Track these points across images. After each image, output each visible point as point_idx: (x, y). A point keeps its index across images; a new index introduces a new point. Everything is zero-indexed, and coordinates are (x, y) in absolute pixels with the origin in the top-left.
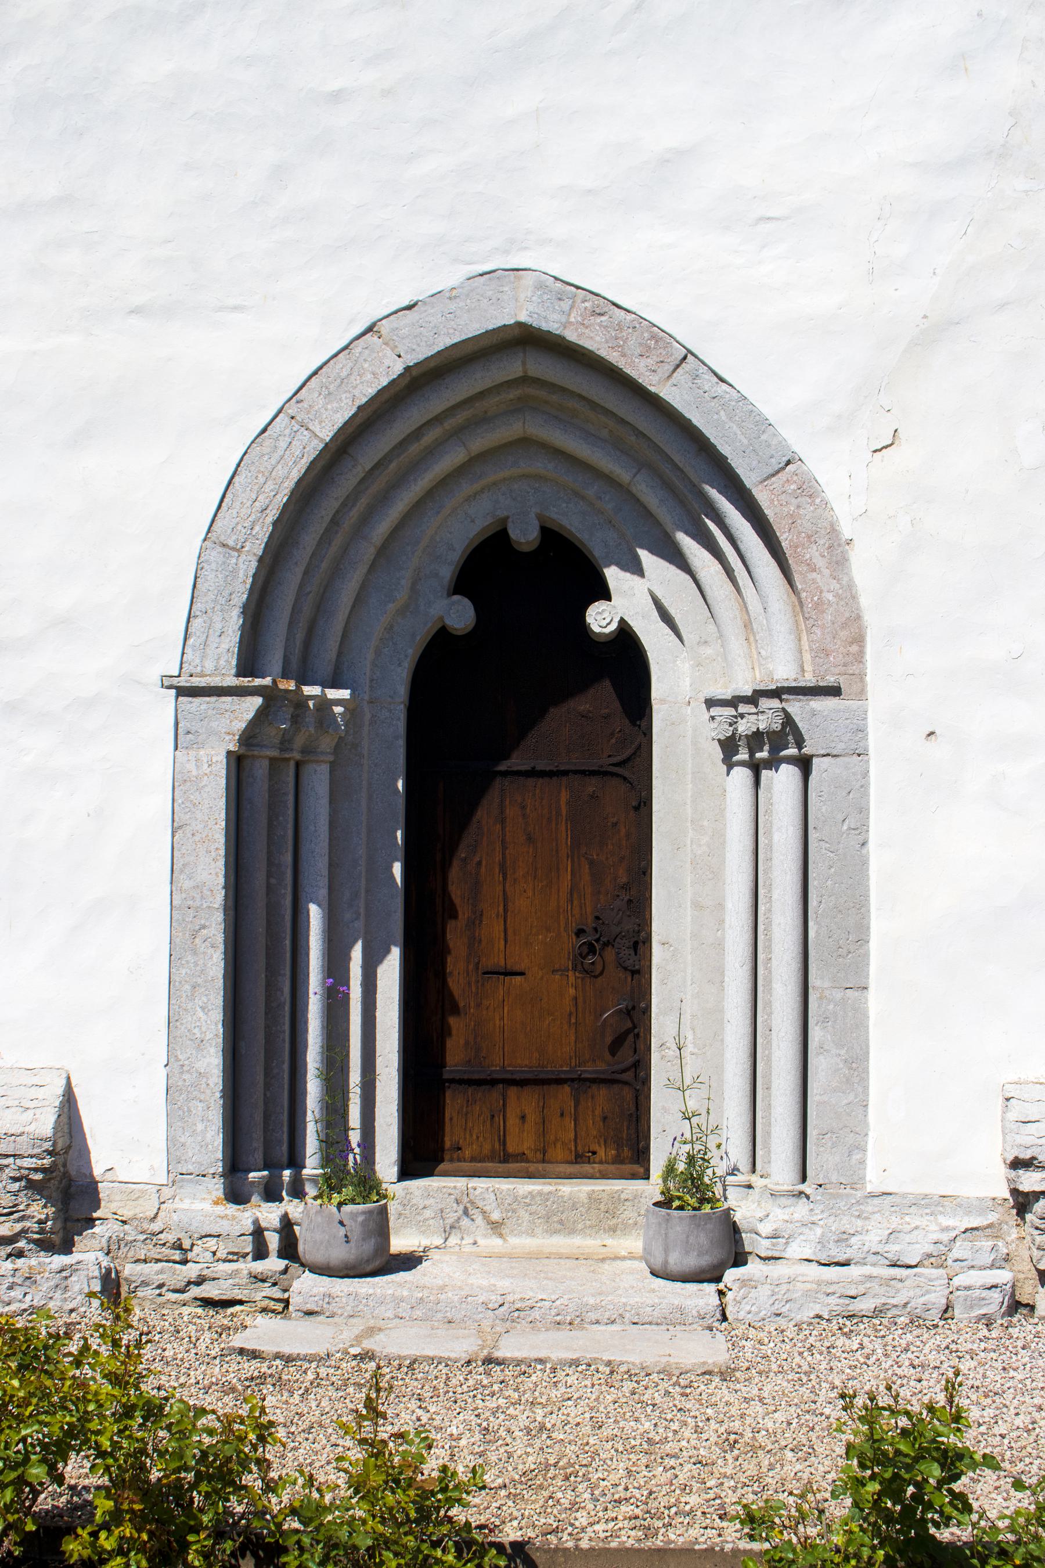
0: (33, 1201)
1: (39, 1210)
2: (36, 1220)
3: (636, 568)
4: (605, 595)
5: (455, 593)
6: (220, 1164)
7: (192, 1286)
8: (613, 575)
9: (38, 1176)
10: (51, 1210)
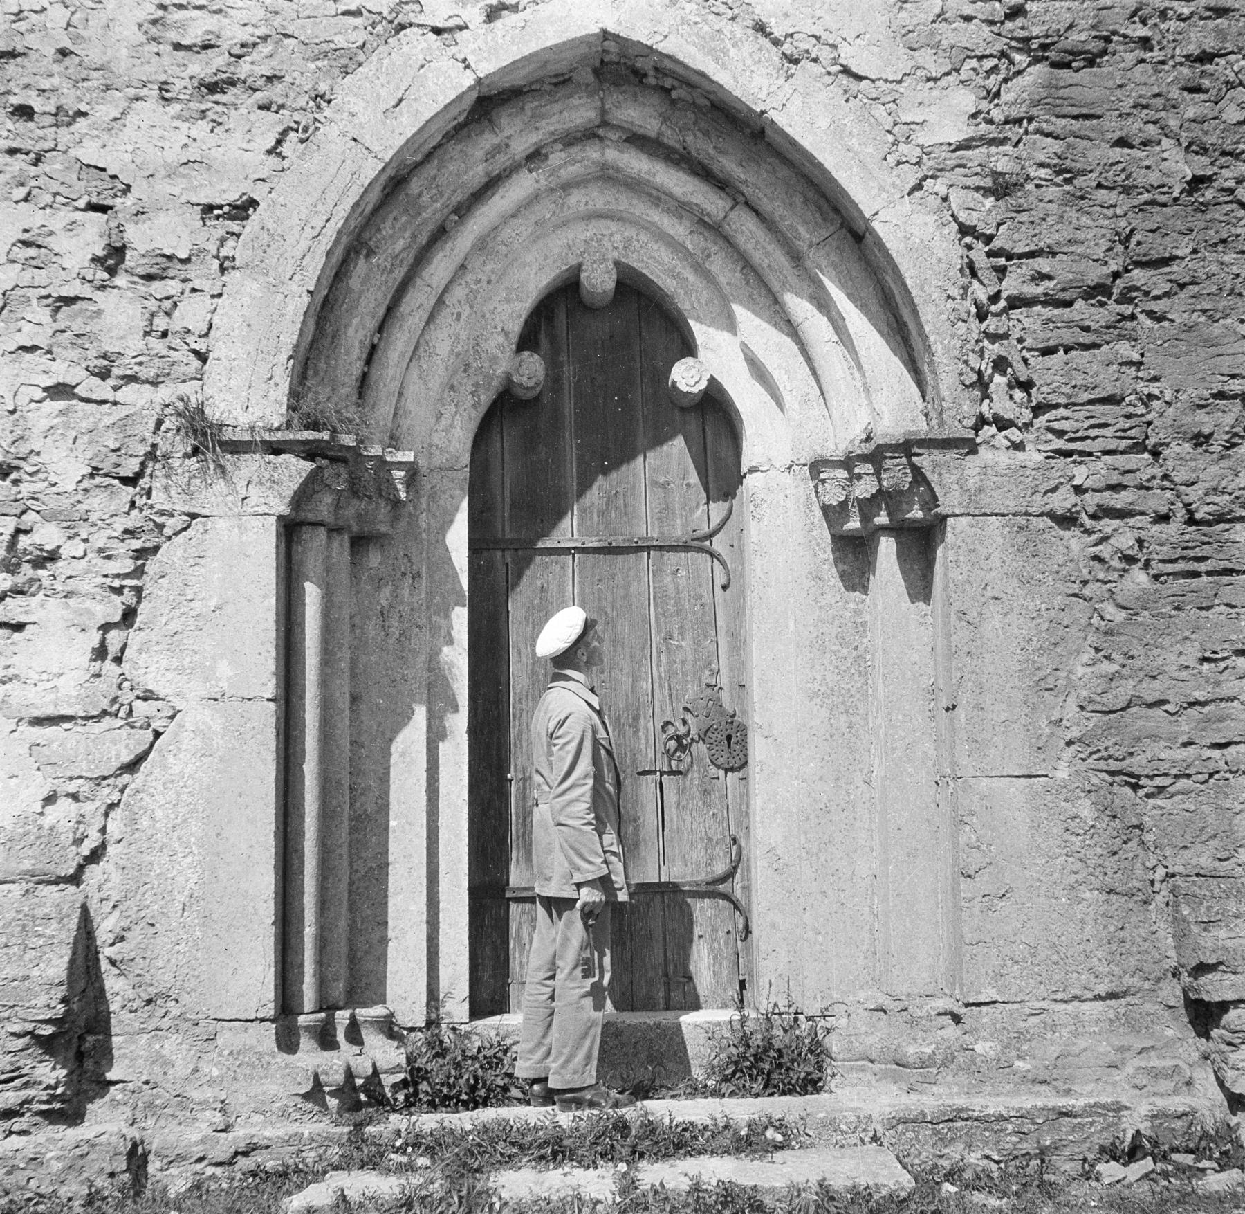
0: (41, 1062)
1: (50, 1073)
2: (44, 1086)
3: (731, 325)
4: (688, 348)
5: (523, 350)
6: (272, 1005)
7: (239, 1157)
8: (699, 330)
9: (47, 1030)
10: (62, 1073)
